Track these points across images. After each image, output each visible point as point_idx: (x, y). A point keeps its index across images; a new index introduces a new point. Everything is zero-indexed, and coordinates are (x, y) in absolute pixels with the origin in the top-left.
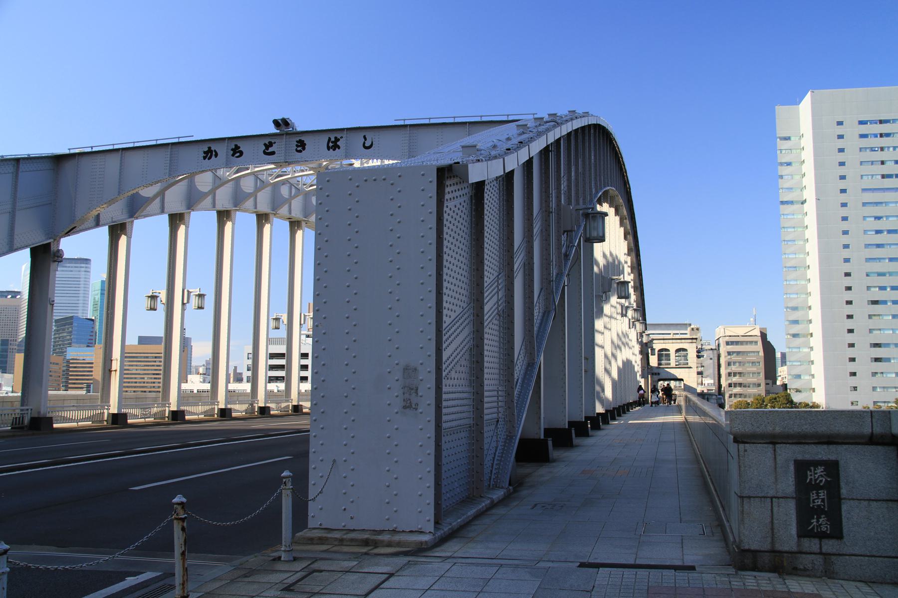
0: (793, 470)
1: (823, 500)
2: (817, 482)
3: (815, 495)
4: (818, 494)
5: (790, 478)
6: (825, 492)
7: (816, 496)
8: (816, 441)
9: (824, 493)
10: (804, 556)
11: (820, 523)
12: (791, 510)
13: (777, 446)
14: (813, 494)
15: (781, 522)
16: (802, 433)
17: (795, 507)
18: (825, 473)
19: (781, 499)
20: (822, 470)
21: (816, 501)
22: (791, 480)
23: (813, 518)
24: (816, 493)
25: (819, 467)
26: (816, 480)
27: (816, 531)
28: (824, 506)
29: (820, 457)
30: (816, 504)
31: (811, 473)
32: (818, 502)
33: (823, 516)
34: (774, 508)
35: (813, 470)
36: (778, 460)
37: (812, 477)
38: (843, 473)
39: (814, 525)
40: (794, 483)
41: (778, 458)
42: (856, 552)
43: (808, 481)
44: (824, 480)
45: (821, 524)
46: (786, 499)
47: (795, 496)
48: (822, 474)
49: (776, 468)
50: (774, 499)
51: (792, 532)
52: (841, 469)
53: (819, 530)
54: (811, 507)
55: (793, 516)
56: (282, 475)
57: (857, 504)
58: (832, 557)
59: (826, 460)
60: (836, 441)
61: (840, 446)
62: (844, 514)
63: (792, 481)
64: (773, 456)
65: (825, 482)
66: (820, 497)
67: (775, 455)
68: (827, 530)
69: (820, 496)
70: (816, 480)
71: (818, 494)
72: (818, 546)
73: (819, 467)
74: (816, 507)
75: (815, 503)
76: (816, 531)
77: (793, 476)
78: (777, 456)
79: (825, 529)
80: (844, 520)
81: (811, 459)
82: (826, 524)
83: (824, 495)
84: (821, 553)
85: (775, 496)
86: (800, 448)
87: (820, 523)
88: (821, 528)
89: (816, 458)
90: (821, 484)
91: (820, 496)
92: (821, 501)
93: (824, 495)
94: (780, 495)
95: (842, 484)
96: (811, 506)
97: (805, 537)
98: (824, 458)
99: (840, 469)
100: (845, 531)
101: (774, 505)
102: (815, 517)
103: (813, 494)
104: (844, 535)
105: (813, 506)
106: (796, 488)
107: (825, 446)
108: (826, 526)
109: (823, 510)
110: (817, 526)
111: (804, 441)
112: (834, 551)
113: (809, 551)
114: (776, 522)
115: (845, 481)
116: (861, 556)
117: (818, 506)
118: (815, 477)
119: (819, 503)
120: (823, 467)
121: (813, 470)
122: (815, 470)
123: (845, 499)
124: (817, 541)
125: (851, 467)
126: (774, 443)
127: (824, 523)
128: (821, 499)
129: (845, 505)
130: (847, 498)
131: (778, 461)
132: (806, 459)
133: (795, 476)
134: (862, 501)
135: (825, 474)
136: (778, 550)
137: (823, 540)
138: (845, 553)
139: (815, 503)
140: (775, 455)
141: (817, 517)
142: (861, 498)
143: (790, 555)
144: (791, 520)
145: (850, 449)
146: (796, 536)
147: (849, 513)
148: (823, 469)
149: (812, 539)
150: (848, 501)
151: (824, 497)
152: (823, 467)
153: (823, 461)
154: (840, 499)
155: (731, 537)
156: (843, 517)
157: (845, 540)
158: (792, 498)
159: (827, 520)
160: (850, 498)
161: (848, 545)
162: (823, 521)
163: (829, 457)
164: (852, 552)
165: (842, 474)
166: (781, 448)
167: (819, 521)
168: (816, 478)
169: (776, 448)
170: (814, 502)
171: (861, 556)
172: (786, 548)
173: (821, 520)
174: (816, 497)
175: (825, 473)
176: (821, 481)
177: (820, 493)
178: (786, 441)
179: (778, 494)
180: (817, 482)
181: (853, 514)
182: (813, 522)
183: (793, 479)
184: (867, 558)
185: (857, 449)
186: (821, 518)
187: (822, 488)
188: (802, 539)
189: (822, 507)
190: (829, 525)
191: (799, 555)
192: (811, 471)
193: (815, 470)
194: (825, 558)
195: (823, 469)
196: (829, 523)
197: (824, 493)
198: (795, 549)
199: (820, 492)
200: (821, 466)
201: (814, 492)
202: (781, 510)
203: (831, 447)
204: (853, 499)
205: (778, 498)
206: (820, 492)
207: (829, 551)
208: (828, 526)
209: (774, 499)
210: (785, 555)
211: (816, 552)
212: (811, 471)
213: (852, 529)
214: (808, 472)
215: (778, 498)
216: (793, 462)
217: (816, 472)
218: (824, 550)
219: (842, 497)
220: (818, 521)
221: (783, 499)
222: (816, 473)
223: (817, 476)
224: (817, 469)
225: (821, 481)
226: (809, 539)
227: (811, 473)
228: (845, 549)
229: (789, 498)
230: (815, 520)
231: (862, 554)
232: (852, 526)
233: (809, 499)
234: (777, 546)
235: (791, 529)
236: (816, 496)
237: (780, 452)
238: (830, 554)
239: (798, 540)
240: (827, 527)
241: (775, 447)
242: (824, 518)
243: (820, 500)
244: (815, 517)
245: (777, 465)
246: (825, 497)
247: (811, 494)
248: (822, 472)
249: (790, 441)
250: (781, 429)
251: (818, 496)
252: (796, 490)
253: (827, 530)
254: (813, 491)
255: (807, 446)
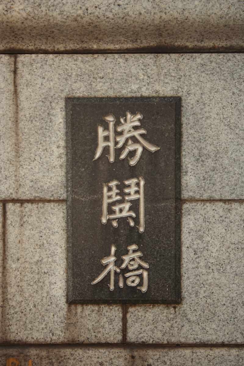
0: (62, 126)
1: (135, 205)
2: (123, 156)
3: (115, 191)
4: (121, 187)
5: (54, 148)
6: (142, 183)
7: (117, 194)
8: (129, 46)
9: (138, 185)
10: (80, 352)
11: (124, 266)
12: (53, 234)
13: (22, 58)
14: (110, 189)
15: (27, 265)
16: (87, 19)
17: (64, 224)
18: (143, 131)
19: (29, 205)
20: (137, 124)
21: (116, 208)
22: (56, 154)
23: (108, 254)
24: (118, 187)
25: (129, 116)
26: (118, 152)
27: (112, 287)
28: (136, 220)
29: (134, 87)
30: (118, 215)
31: (106, 133)
32: (121, 211)
33: (134, 247)
34: (10, 229)
35: (111, 125)
36: (22, 97)
37: (111, 144)
38: (191, 131)
39: (109, 273)
40: (64, 159)
41: (24, 93)
42: (210, 338)
43: (98, 155)
44: (140, 150)
45: (127, 270)
46: (41, 205)
47: (64, 196)
48: (136, 134)
49: (16, 122)
50: (10, 206)
51: (54, 292)
52: (187, 119)
53: (121, 285)
54: (102, 225)
55: (60, 250)
56: (126, 275)
57: (221, 213)
58: (150, 352)
59: (148, 98)
60: (178, 43)
61: (188, 56)
62: (186, 238)
63: (60, 157)
64: (12, 88)
65: (141, 157)
66: (127, 198)
67: (15, 86)
68: (141, 284)
69: (129, 194)
70: (118, 152)
71: (121, 187)
72: (118, 325)
73: (129, 116)
74: (115, 224)
75: (113, 212)
76: (112, 287)
77: (62, 143)
78: (19, 89)
79: (137, 281)
80: (187, 255)
81: (111, 94)
82: (140, 267)
83: (137, 192)
84: (124, 344)
85: (14, 196)
86: (82, 65)
87: (124, 266)
88: (125, 279)
89: (124, 92)
90: (133, 163)
91: (129, 194)
92: (130, 209)
93: (137, 192)
94: (26, 193)
95: (187, 161)
96: (104, 221)
97: (84, 302)
98: (146, 92)
99: (184, 120)
100: (187, 283)
101: (9, 222)
102: (113, 249)
103: (110, 189)
104: (185, 294)
105: (109, 221)
106: (67, 173)
107: (149, 58)
108: (140, 272)
109: (134, 229)
110: (116, 272)
111: (95, 47)
112: (158, 336)
113: (94, 340)
114: (14, 266)
115: (196, 151)
116: (223, 345)
117: (123, 221)
118: (116, 143)
119: (125, 214)
120: (139, 116)
121: (111, 125)
122: (118, 123)
123: (192, 200)
124: (115, 312)
125: (214, 115)
126: (13, 53)
127: (136, 266)
128: (131, 201)
129: (192, 217)
130: (198, 197)
131: (24, 104)
132: (99, 95)
133: (67, 141)
134: (235, 205)
135: (142, 135)
136: (18, 338)
137: (131, 309)
138: (183, 340)
139: (113, 212)
140: (15, 86)
141: (116, 252)
142: (234, 197)
143: (44, 353)
144: (54, 261)
145: (214, 64)
146: (64, 300)
147: (201, 238)
148: (139, 120)
149: (105, 309)
150: (199, 206)
151: (136, 197)
152: (139, 116)
153: (142, 98)
154: (179, 201)
155: (105, 273)
156: (184, 249)
157: (185, 306)
158: (59, 201)
159: (140, 258)
160: (205, 196)
161: (193, 318)
162: (133, 259)
163: (157, 87)
164: (202, 337)
165: (188, 132)
166: (31, 64)
167: (122, 261)
168: (120, 145)
169: (20, 65)
170: (111, 212)
171: (223, 345)
172: (38, 336)
173: (126, 258)
174: (118, 198)
175: (143, 131)
176: (132, 154)
177: (129, 186)
178: (49, 48)
179: (21, 190)
180: (123, 156)
181: (209, 239)
182: (107, 266)
183: (62, 151)
184: (234, 351)
185: (230, 63)
186: (127, 252)
187: (133, 172)
188: (79, 308)
189: (132, 224)
190: (147, 270)
191: (68, 351)
192: (106, 128)
193: (118, 123)
194: (133, 357)
195: (139, 120)
196: (146, 265)
197: (138, 185)
198: (60, 336)
199: (127, 183)
200: (134, 113)
201: (113, 184)
202: (27, 233)
203: (164, 58)
204: (211, 200)
205: (22, 202)
206: (127, 183)
207: (146, 337)
208: (145, 274)
209: (10, 206)
210: (33, 352)
211: (111, 340)
212: (106, 128)
213: (205, 277)
214: (100, 130)
215: (22, 202)
216: (62, 104)
217: (119, 129)
218: (132, 336)
219: (185, 194)
220: (118, 262)
221: (35, 206)
222: (121, 133)
223: (121, 140)
224: (122, 120)
225: (132, 154)
226: (96, 308)
227: (106, 133)
228: (185, 330)
229: (49, 201)
230: (112, 259)
231: (226, 340)
232: (204, 271)
233: (99, 202)
234: (14, 328)
235: (50, 283)
236: (117, 194)
237: (29, 77)
238: (144, 346)
239: (69, 310)
240: (141, 276)
241: (15, 63)
242: (134, 251)
243: (127, 206)
244: (113, 249)
245: (21, 114)
246: (141, 196)
247: (105, 189)
248: (136, 128)
249: (61, 47)
250: (29, 9)
251: (122, 194)
252: (67, 180)
253: (141, 284)
254: (109, 181)
255: (100, 59)
